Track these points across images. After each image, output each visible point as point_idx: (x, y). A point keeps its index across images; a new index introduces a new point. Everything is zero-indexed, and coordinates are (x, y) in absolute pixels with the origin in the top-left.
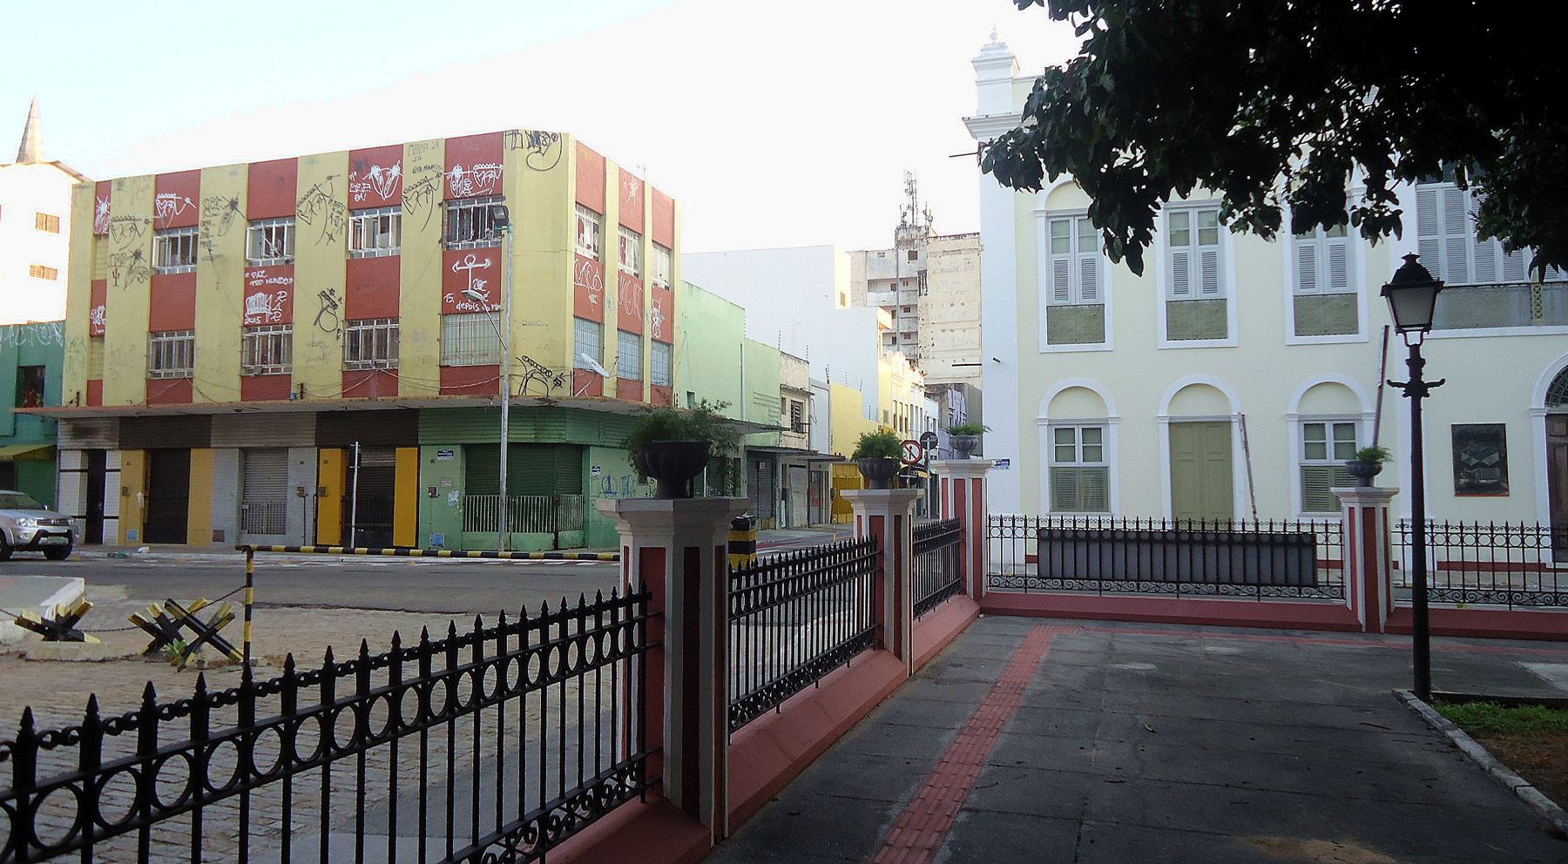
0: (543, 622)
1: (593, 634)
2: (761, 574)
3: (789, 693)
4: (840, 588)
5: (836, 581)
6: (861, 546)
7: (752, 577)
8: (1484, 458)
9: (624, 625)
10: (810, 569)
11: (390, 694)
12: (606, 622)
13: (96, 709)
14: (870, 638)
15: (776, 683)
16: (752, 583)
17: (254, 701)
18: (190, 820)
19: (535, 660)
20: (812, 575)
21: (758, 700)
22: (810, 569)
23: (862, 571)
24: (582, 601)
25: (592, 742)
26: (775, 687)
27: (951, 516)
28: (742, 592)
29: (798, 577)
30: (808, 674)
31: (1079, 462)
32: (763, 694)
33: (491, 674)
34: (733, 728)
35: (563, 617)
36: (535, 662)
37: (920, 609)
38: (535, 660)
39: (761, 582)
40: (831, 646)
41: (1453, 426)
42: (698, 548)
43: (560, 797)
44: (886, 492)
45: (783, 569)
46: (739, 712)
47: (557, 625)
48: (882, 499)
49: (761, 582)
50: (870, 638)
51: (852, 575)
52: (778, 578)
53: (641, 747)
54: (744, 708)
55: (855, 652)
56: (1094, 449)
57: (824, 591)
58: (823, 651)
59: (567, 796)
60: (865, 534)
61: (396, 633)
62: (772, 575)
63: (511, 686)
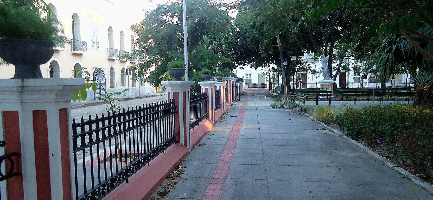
0: (90, 123)
1: (80, 135)
2: (135, 113)
3: (167, 147)
4: (171, 117)
5: (173, 113)
6: (169, 103)
7: (139, 113)
8: (203, 80)
9: (118, 124)
10: (159, 109)
11: (89, 133)
12: (112, 122)
13: (83, 120)
14: (174, 140)
15: (156, 149)
16: (131, 117)
17: (104, 121)
18: (90, 148)
19: (87, 137)
20: (165, 110)
21: (164, 145)
22: (159, 109)
23: (169, 114)
24: (82, 119)
25: (97, 170)
26: (155, 150)
27: (204, 92)
28: (105, 128)
29: (157, 112)
30: (153, 154)
31: (248, 78)
32: (130, 167)
33: (87, 137)
34: (150, 160)
35: (114, 117)
36: (87, 137)
37: (192, 126)
38: (87, 137)
39: (135, 117)
40: (169, 138)
41: (3, 111)
42: (185, 92)
43: (105, 180)
44: (210, 82)
45: (145, 111)
46: (143, 161)
47: (95, 124)
48: (208, 84)
49: (135, 117)
50: (174, 140)
51: (166, 115)
52: (162, 109)
53: (175, 134)
54: (153, 153)
55: (167, 147)
56: (250, 77)
57: (163, 119)
58: (171, 136)
59: (102, 184)
60: (171, 98)
61: (90, 115)
62: (155, 109)
63: (101, 138)
